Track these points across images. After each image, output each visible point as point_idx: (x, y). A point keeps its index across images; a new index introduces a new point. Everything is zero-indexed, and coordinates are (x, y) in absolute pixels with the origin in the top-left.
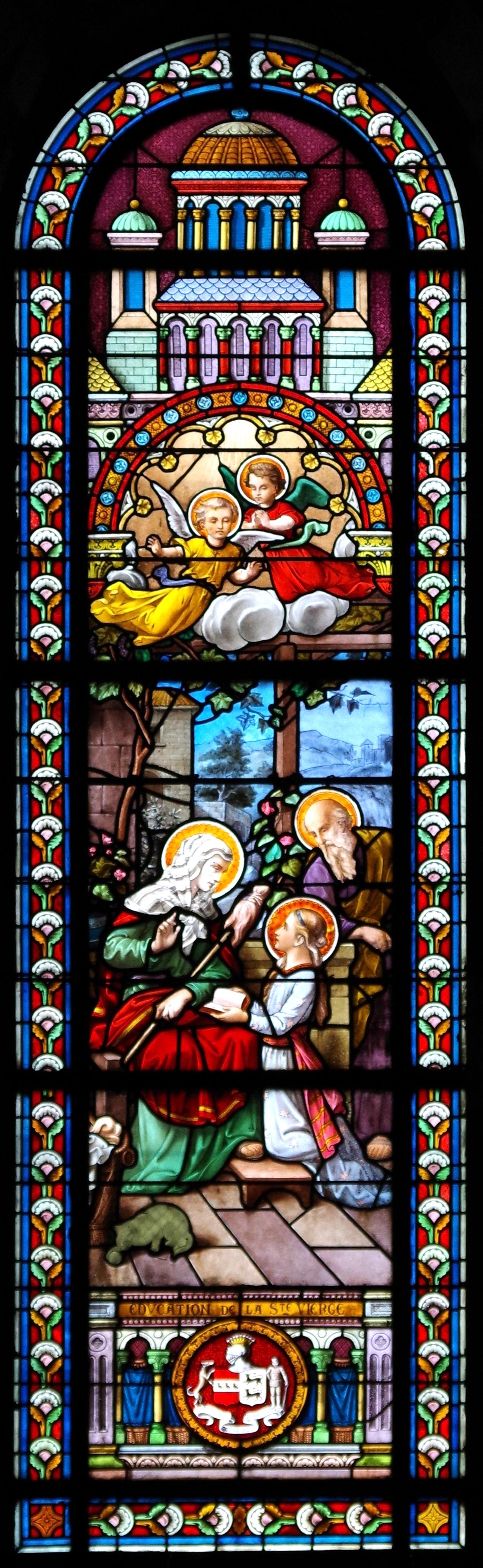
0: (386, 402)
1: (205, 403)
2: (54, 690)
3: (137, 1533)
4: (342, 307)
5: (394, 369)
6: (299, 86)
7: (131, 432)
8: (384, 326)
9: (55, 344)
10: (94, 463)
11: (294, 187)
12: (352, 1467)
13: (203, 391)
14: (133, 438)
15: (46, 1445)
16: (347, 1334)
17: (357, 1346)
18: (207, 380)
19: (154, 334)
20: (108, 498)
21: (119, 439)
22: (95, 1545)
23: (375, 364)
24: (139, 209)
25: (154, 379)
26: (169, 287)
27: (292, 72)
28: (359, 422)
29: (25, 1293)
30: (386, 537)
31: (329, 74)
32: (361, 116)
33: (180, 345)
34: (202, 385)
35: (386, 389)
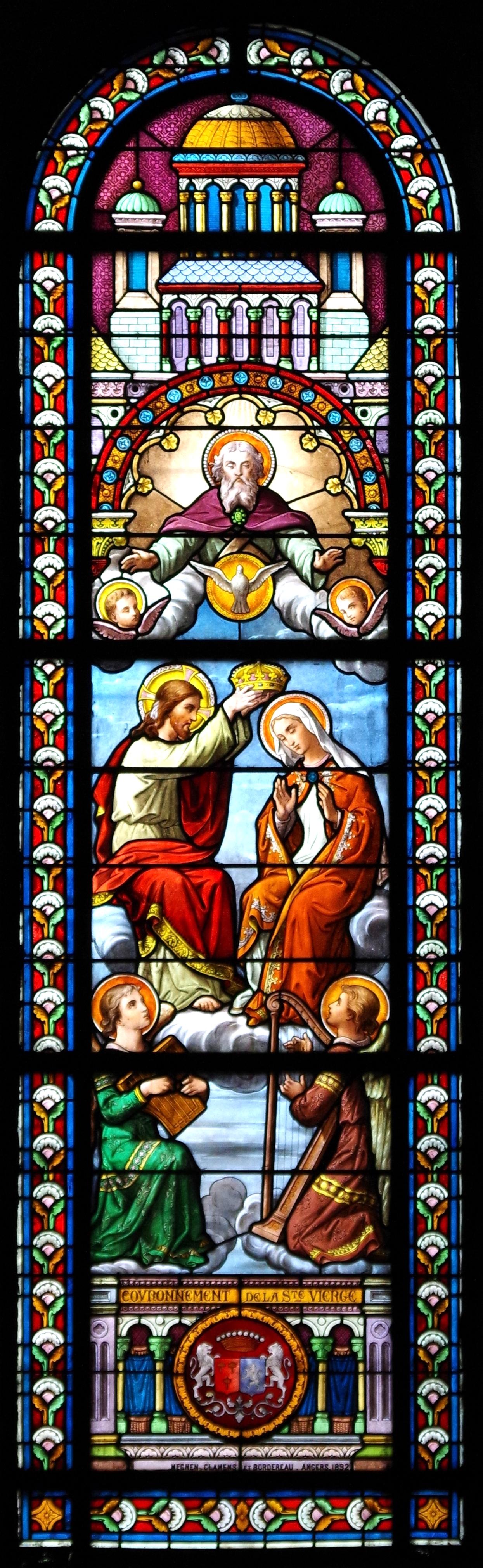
0: (382, 381)
1: (207, 385)
2: (57, 668)
3: (140, 1529)
4: (135, 288)
5: (390, 349)
6: (297, 72)
7: (134, 411)
8: (379, 306)
9: (58, 324)
10: (97, 445)
11: (293, 169)
12: (353, 1458)
13: (205, 371)
14: (137, 416)
15: (50, 1435)
16: (347, 1321)
17: (357, 1334)
18: (208, 361)
19: (157, 314)
20: (109, 476)
21: (123, 418)
22: (98, 1540)
23: (371, 344)
24: (142, 191)
25: (158, 359)
26: (170, 269)
27: (289, 58)
28: (355, 401)
29: (27, 1281)
30: (381, 518)
31: (325, 60)
32: (356, 101)
33: (180, 326)
34: (203, 366)
35: (382, 369)
